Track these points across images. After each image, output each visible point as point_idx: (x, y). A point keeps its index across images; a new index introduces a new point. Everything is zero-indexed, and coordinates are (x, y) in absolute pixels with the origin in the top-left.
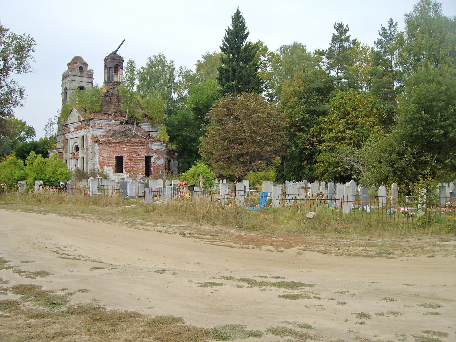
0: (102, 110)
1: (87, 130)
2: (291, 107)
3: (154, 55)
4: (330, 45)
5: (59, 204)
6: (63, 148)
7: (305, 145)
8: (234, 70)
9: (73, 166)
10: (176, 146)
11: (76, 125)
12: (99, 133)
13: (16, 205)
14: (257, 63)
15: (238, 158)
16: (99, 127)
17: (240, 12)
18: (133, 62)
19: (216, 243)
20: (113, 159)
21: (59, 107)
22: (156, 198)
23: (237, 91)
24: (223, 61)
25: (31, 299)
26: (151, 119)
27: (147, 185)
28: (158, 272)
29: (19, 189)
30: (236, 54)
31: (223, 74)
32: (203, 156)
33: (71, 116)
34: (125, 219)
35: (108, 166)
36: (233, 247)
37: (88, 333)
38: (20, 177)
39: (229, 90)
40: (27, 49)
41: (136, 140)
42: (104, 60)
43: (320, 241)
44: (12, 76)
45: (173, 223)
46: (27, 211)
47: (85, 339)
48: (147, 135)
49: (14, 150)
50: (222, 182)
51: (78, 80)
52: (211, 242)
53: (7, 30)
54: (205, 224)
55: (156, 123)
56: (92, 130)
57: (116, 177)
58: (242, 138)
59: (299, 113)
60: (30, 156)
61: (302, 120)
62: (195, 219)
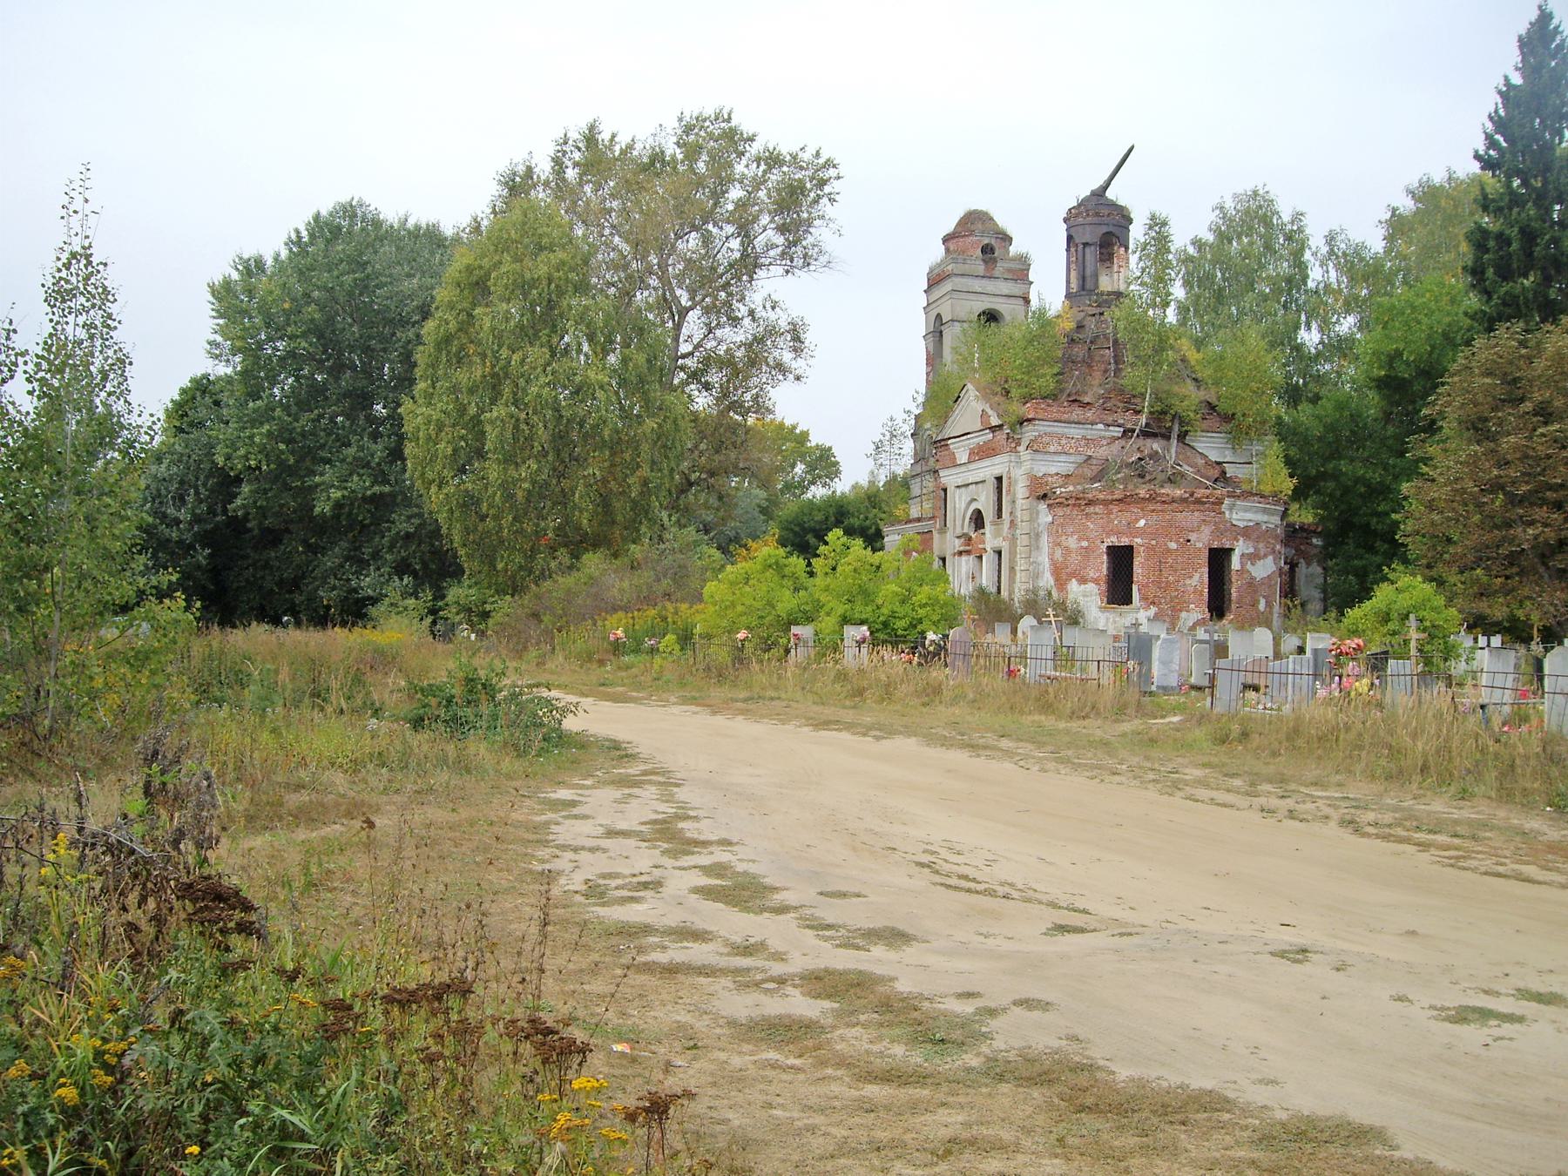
0: (1062, 391)
1: (1013, 458)
3: (1235, 196)
5: (924, 705)
6: (930, 519)
8: (1529, 236)
9: (964, 576)
10: (1316, 515)
11: (975, 440)
12: (1053, 466)
13: (784, 704)
15: (1543, 556)
16: (1052, 449)
17: (1550, 16)
18: (1164, 224)
20: (1100, 556)
22: (1251, 695)
23: (1539, 311)
24: (1485, 204)
25: (862, 1018)
26: (1228, 418)
27: (1220, 650)
28: (1282, 954)
29: (793, 651)
30: (1536, 177)
31: (1487, 251)
32: (1415, 547)
33: (959, 409)
34: (1149, 765)
35: (1083, 581)
36: (1539, 883)
37: (1059, 1151)
39: (1511, 309)
40: (812, 195)
41: (1178, 492)
42: (1065, 220)
44: (770, 284)
45: (1316, 784)
47: (1048, 1169)
48: (1216, 473)
50: (1488, 645)
51: (980, 290)
53: (751, 139)
54: (1429, 793)
55: (1247, 434)
57: (1108, 619)
60: (826, 543)
62: (1394, 772)
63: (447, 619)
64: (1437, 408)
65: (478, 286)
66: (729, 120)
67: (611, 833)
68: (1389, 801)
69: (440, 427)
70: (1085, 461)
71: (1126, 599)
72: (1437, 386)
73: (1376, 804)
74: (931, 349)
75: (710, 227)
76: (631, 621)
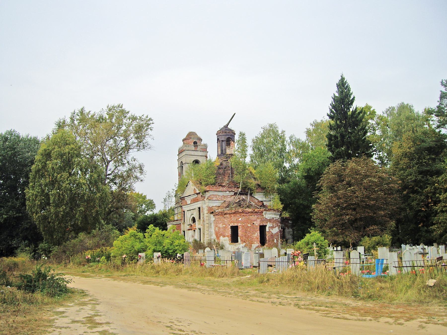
0: (217, 182)
2: (403, 169)
4: (439, 103)
7: (420, 207)
8: (343, 136)
9: (190, 236)
12: (214, 204)
13: (135, 276)
14: (365, 126)
16: (214, 199)
17: (344, 79)
18: (244, 135)
19: (331, 315)
20: (228, 229)
21: (176, 181)
22: (270, 268)
26: (263, 188)
27: (262, 255)
29: (139, 260)
31: (332, 140)
32: (317, 223)
34: (240, 291)
35: (224, 236)
36: (350, 319)
38: (140, 249)
40: (145, 128)
43: (444, 312)
44: (133, 153)
46: (145, 282)
48: (261, 204)
49: (136, 222)
51: (193, 154)
52: (326, 314)
53: (128, 113)
54: (320, 295)
56: (208, 202)
57: (231, 247)
58: (355, 204)
59: (411, 175)
61: (415, 181)
62: (310, 289)
63: (39, 253)
64: (320, 184)
65: (48, 155)
66: (122, 107)
67: (74, 322)
68: (308, 298)
69: (36, 196)
71: (237, 241)
72: (320, 178)
73: (305, 299)
74: (180, 172)
75: (116, 137)
76: (92, 253)
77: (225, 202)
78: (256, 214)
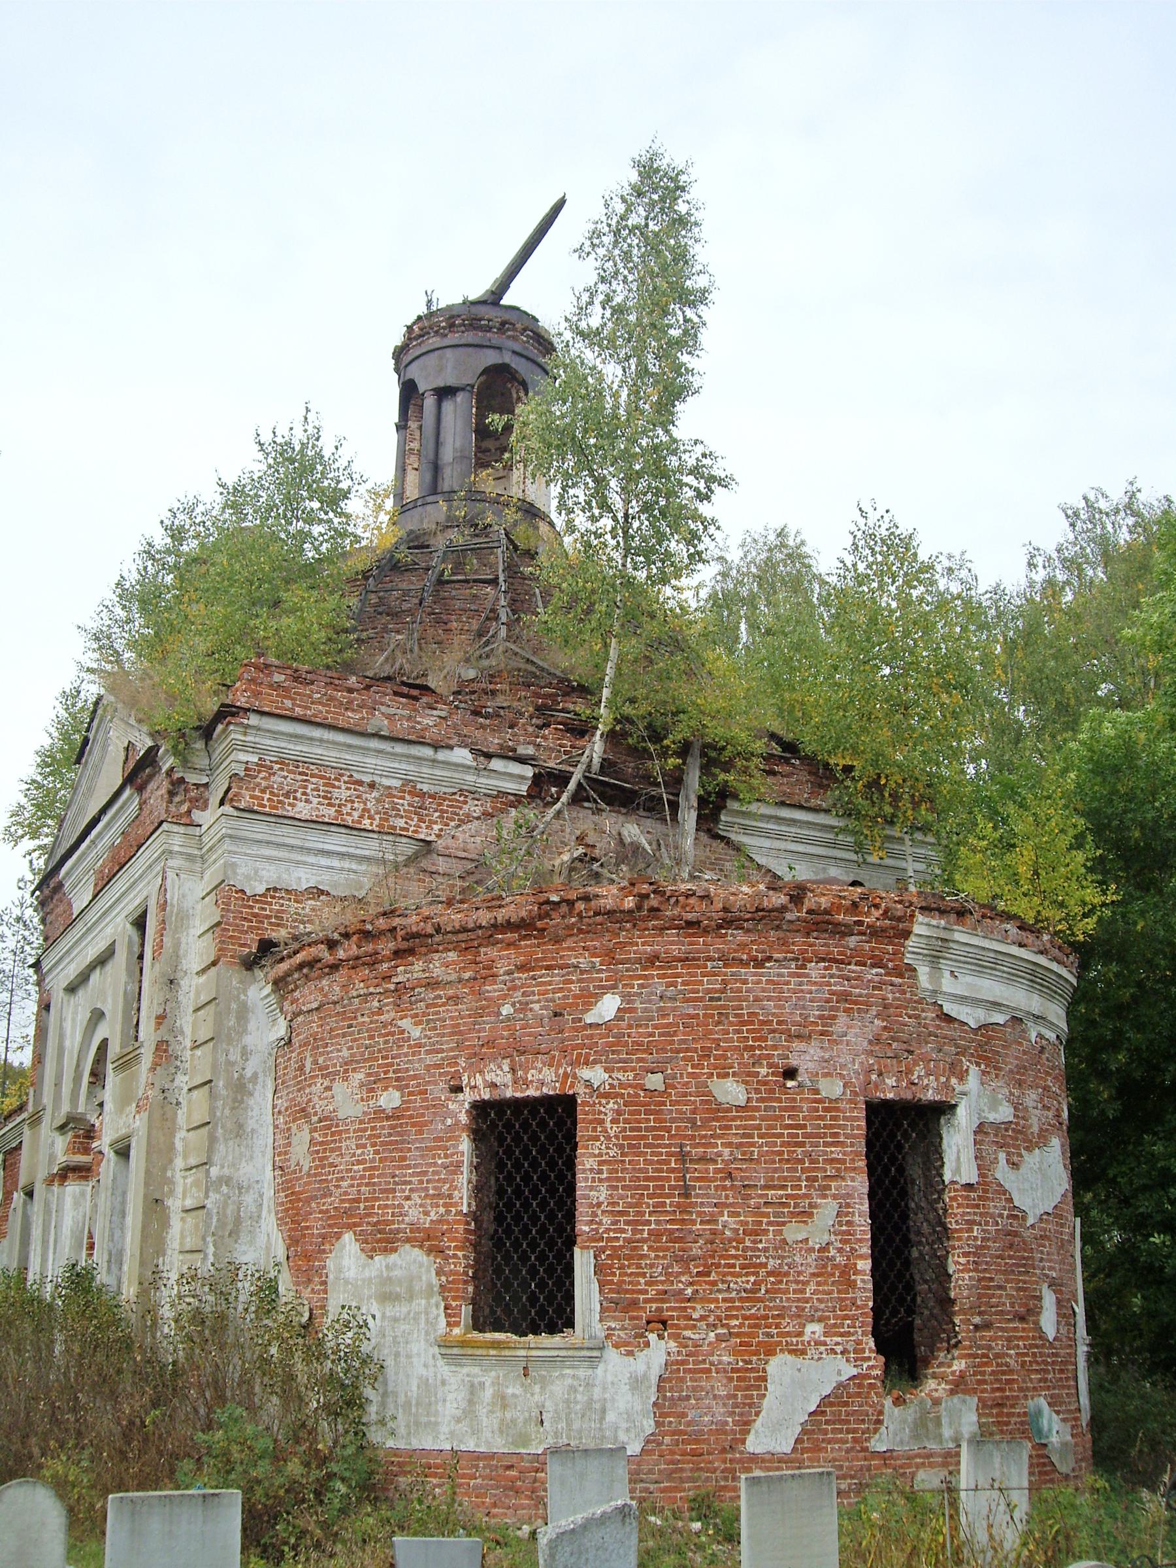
16: (303, 810)
20: (443, 1142)
57: (474, 1389)
70: (411, 860)
77: (424, 864)
78: (820, 943)
